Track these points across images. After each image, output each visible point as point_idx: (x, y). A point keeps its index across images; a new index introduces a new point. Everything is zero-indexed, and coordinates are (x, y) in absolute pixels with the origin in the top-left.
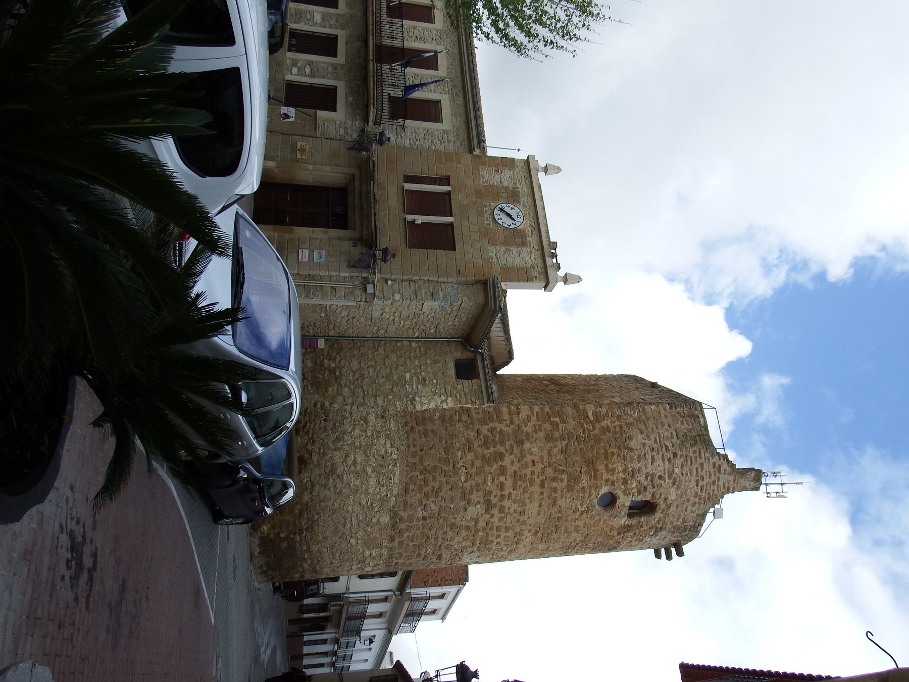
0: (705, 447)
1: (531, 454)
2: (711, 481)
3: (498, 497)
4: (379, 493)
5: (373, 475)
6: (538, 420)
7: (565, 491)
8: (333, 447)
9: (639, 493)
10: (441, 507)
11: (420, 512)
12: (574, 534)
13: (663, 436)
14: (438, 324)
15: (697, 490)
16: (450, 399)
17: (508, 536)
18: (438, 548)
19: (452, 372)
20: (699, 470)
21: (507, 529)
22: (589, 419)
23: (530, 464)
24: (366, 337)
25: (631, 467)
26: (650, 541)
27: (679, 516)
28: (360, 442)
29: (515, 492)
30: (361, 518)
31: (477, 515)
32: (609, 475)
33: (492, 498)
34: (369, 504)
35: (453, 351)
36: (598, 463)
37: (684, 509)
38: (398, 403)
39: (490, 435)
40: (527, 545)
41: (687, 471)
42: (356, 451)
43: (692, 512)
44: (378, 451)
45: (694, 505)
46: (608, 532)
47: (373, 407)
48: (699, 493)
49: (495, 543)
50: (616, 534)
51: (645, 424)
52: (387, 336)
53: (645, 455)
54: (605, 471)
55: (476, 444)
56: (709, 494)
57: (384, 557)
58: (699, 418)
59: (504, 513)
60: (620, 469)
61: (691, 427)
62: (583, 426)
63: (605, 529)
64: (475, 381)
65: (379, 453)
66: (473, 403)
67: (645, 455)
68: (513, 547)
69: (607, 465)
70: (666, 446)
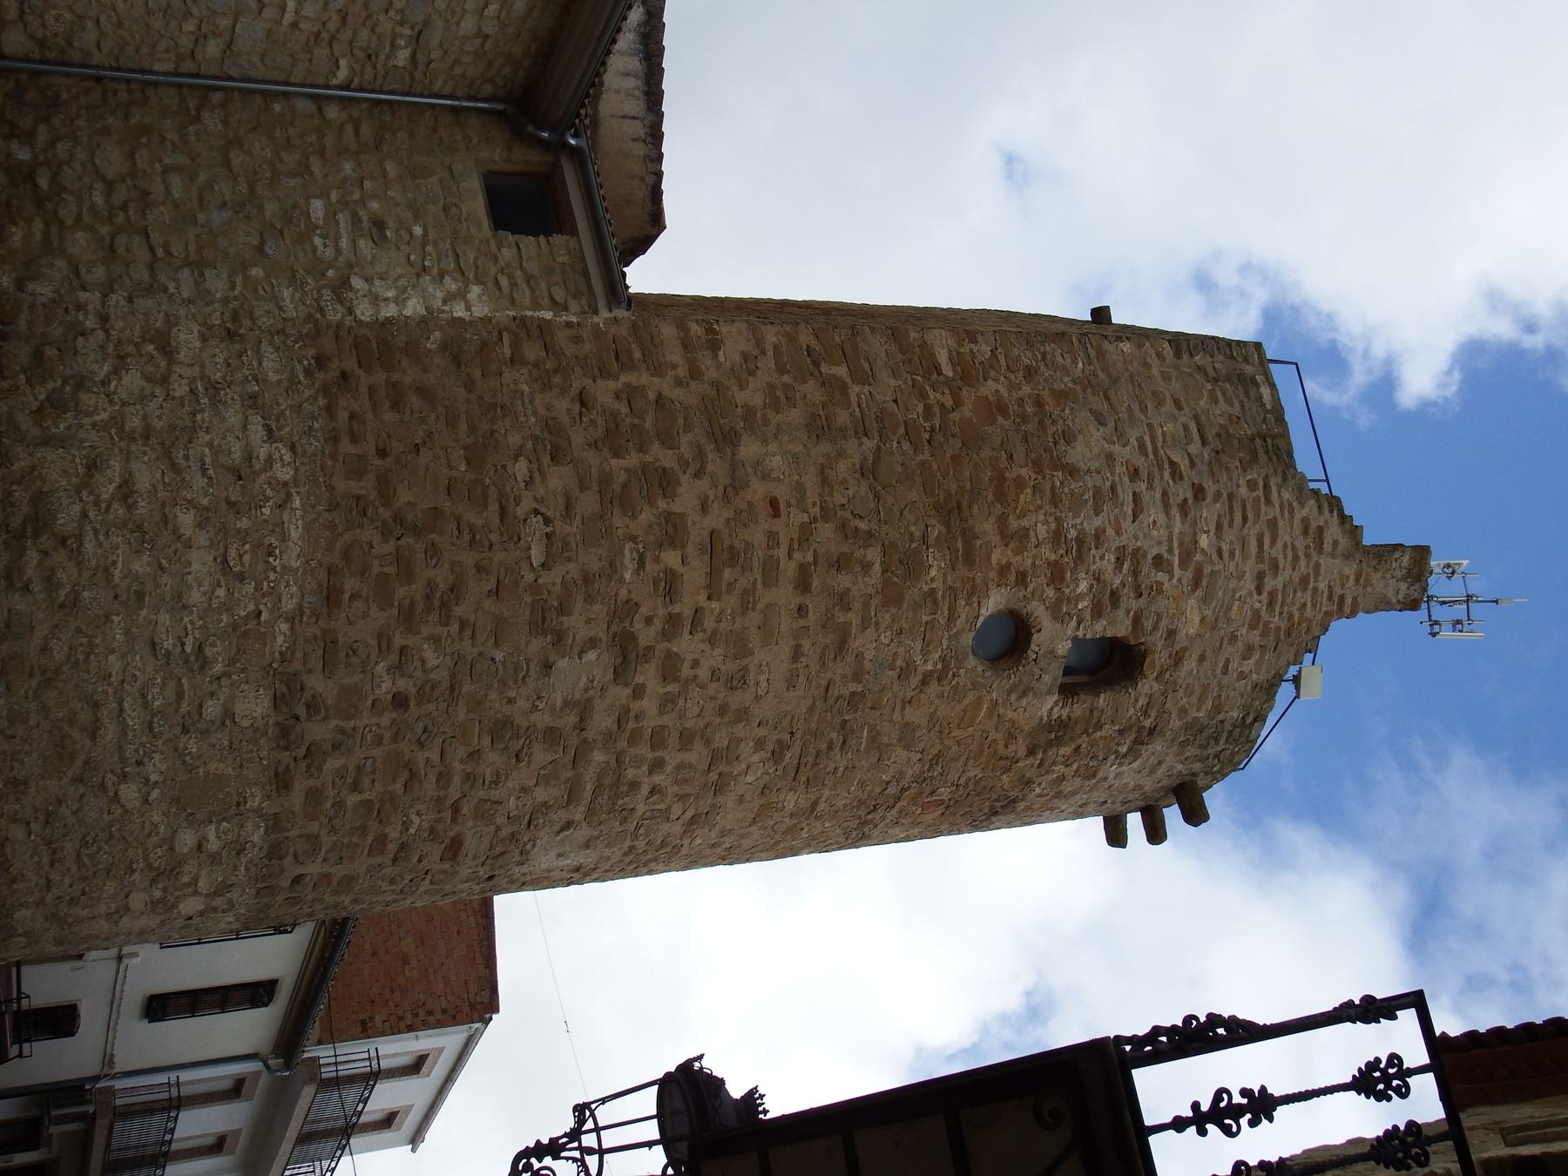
0: (1279, 471)
1: (765, 477)
2: (1296, 576)
3: (658, 624)
4: (227, 607)
5: (202, 538)
6: (781, 369)
7: (875, 602)
8: (35, 431)
9: (1097, 612)
10: (459, 658)
11: (386, 678)
12: (900, 754)
13: (1164, 434)
14: (426, 23)
15: (1257, 605)
16: (476, 290)
17: (691, 766)
18: (448, 815)
19: (477, 205)
20: (1267, 541)
21: (686, 739)
22: (940, 373)
23: (763, 510)
24: (150, 72)
25: (1074, 526)
26: (1117, 775)
27: (1205, 687)
28: (145, 417)
29: (715, 605)
30: (157, 703)
31: (587, 690)
32: (1009, 552)
33: (638, 626)
34: (188, 649)
35: (475, 141)
36: (975, 510)
37: (1220, 665)
38: (287, 293)
39: (624, 410)
40: (748, 797)
41: (1231, 542)
42: (129, 453)
43: (1242, 676)
44: (216, 451)
45: (1249, 651)
46: (1002, 744)
47: (191, 301)
48: (1264, 614)
49: (645, 790)
50: (1022, 751)
51: (1107, 397)
52: (233, 72)
53: (1113, 489)
54: (998, 538)
55: (578, 438)
56: (1289, 620)
57: (252, 853)
58: (1257, 385)
59: (676, 679)
60: (1042, 530)
61: (1237, 410)
62: (923, 395)
63: (993, 735)
64: (557, 239)
65: (222, 459)
66: (555, 305)
67: (1113, 489)
68: (704, 805)
69: (1002, 521)
70: (1172, 464)
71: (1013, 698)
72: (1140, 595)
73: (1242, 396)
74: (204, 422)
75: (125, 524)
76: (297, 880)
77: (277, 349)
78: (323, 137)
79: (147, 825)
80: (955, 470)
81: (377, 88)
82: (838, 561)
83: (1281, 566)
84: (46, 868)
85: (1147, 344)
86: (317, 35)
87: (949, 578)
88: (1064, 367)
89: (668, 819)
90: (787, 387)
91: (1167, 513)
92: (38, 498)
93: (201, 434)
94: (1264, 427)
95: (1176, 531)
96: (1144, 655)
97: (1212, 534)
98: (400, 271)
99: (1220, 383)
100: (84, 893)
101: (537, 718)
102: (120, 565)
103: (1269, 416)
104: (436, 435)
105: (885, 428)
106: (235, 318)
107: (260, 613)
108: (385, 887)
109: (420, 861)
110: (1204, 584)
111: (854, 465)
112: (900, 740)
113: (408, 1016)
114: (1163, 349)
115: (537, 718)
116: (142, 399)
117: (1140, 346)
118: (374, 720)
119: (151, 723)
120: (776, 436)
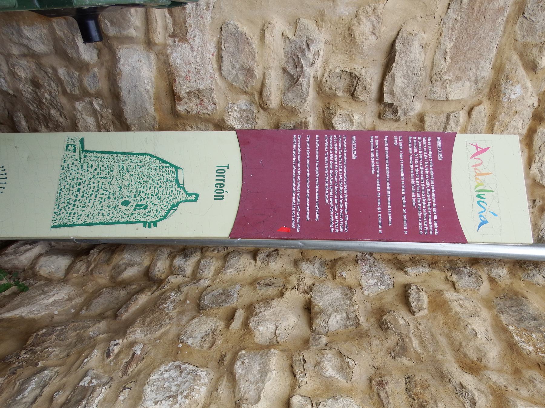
9: (141, 200)
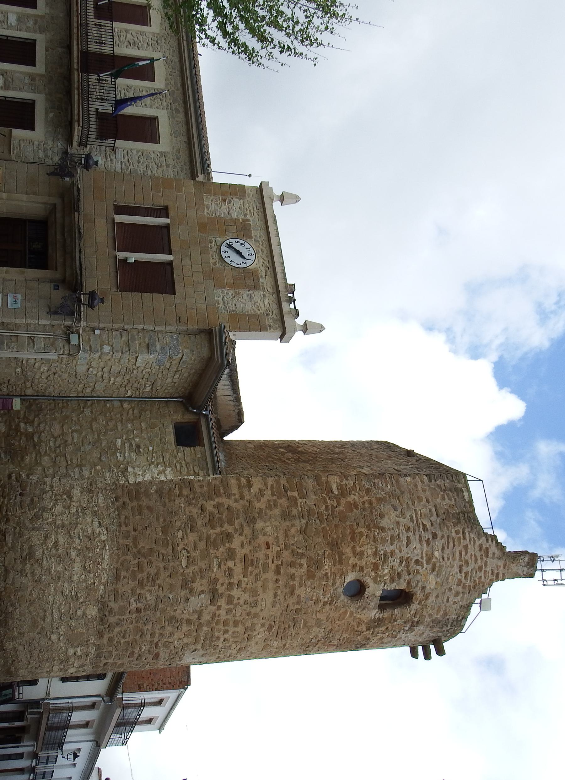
0: (470, 527)
1: (265, 534)
3: (225, 586)
4: (85, 581)
5: (78, 559)
6: (273, 494)
7: (304, 578)
8: (30, 526)
9: (392, 580)
11: (134, 603)
12: (316, 629)
13: (421, 513)
15: (460, 577)
16: (168, 469)
19: (171, 437)
20: (463, 554)
21: (236, 623)
22: (333, 493)
23: (263, 546)
24: (69, 397)
25: (383, 549)
26: (405, 637)
27: (440, 607)
29: (245, 579)
30: (63, 611)
31: (201, 607)
32: (356, 560)
33: (218, 586)
34: (73, 594)
35: (172, 413)
36: (343, 545)
38: (107, 475)
39: (216, 512)
40: (259, 642)
41: (448, 554)
43: (455, 603)
44: (83, 530)
45: (457, 594)
47: (78, 479)
49: (222, 640)
50: (364, 629)
51: (399, 499)
52: (95, 395)
53: (399, 535)
55: (199, 522)
58: (463, 492)
60: (369, 552)
61: (453, 502)
62: (325, 502)
63: (352, 623)
64: (198, 448)
65: (85, 533)
66: (196, 474)
67: (399, 535)
68: (244, 644)
69: (354, 548)
70: (423, 525)
71: (359, 610)
72: (410, 574)
73: (456, 497)
74: (80, 521)
75: (56, 555)
76: (105, 664)
77: (103, 495)
78: (122, 415)
79: (59, 647)
80: (336, 530)
81: (140, 396)
82: (290, 564)
83: (469, 563)
84: (29, 659)
85: (417, 477)
86: (121, 385)
87: (333, 569)
88: (382, 489)
89: (231, 649)
90: (275, 501)
91: (421, 544)
92: (31, 547)
93: (79, 525)
94: (464, 509)
95: (425, 550)
96: (413, 595)
97: (440, 551)
98: (144, 464)
99: (447, 492)
100: (40, 666)
101: (184, 616)
102: (53, 568)
103: (466, 504)
104: (152, 523)
105: (310, 515)
106: (91, 485)
107: (95, 583)
108: (134, 666)
109: (145, 659)
110: (437, 570)
111: (297, 529)
112: (315, 624)
113: (156, 684)
114: (424, 479)
115: (184, 616)
116: (62, 514)
117: (414, 478)
118: (130, 616)
119: (61, 616)
120: (269, 519)
